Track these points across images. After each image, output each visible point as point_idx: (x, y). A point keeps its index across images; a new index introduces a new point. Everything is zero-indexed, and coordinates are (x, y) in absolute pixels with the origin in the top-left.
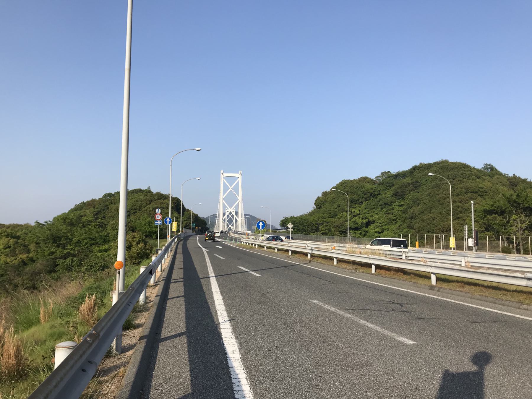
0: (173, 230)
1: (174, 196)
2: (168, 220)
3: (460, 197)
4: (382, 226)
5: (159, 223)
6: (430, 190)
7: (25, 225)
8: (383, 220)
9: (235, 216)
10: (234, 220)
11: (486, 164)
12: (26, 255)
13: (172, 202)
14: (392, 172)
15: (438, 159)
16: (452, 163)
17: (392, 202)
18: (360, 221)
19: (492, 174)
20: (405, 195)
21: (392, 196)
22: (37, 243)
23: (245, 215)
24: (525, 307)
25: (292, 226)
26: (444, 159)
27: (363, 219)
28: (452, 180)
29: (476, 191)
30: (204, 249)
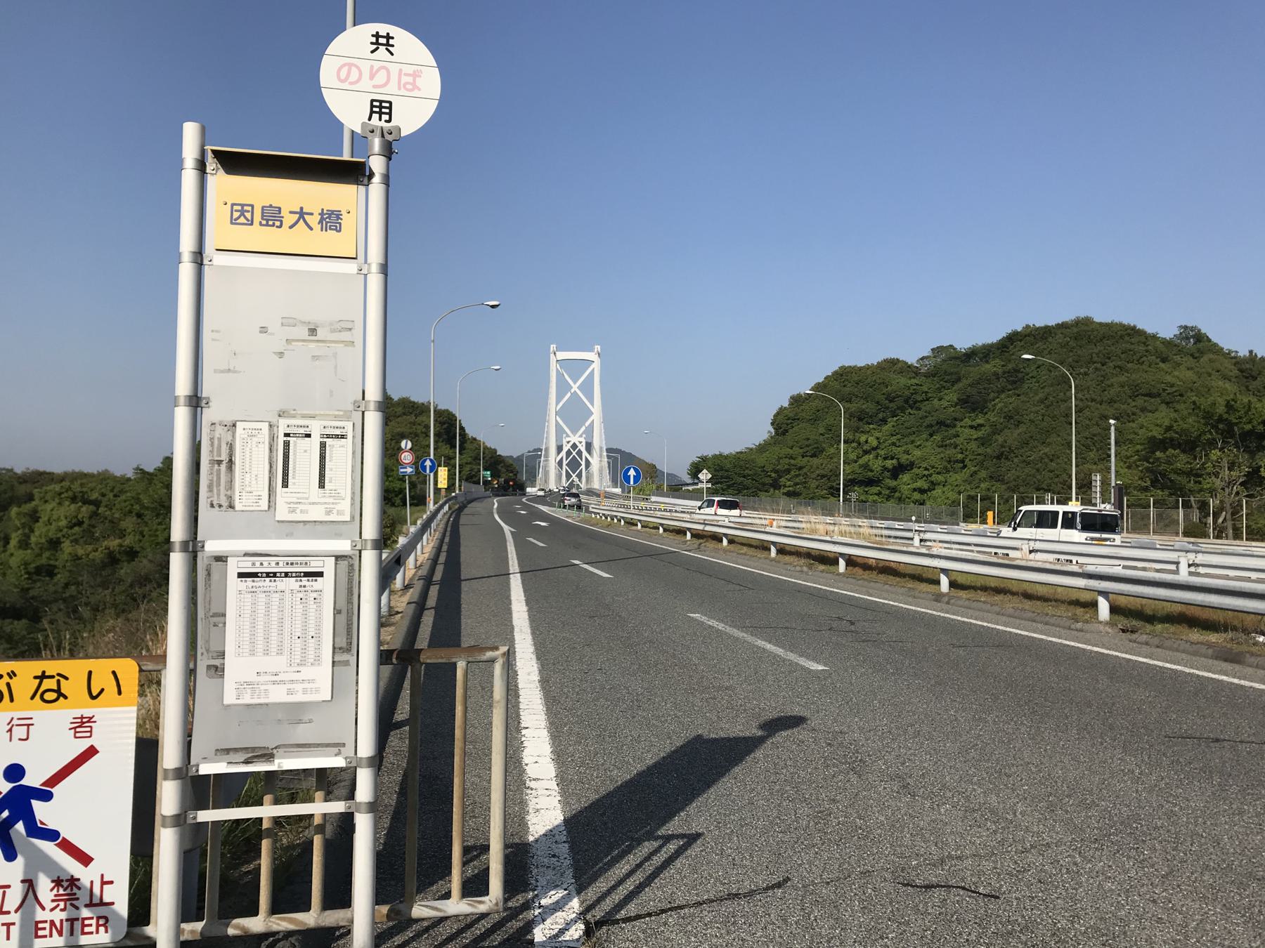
0: (440, 486)
1: (441, 407)
2: (428, 463)
3: (1116, 405)
4: (931, 475)
5: (409, 470)
6: (1046, 390)
7: (99, 474)
8: (934, 460)
9: (585, 454)
10: (583, 463)
11: (1186, 327)
12: (117, 541)
13: (435, 421)
14: (958, 346)
15: (1067, 316)
16: (1100, 324)
17: (956, 419)
18: (877, 465)
19: (1199, 350)
20: (986, 402)
21: (956, 404)
22: (139, 516)
23: (608, 450)
24: (1079, 625)
25: (710, 476)
26: (1082, 315)
27: (885, 459)
28: (1099, 365)
29: (1155, 391)
30: (506, 528)
